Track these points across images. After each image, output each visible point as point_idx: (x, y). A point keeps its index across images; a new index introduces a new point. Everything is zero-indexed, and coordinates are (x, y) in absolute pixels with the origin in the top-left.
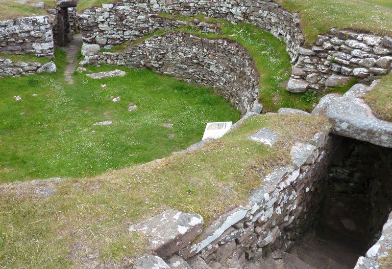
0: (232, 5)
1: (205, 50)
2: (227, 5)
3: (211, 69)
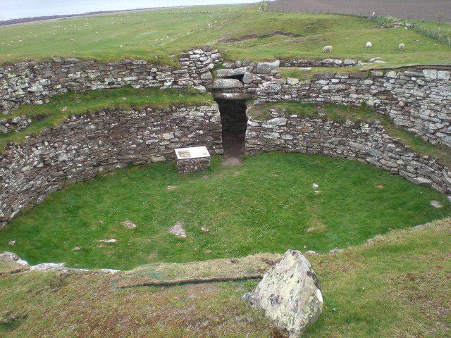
0: (28, 83)
1: (46, 144)
2: (23, 86)
3: (61, 159)
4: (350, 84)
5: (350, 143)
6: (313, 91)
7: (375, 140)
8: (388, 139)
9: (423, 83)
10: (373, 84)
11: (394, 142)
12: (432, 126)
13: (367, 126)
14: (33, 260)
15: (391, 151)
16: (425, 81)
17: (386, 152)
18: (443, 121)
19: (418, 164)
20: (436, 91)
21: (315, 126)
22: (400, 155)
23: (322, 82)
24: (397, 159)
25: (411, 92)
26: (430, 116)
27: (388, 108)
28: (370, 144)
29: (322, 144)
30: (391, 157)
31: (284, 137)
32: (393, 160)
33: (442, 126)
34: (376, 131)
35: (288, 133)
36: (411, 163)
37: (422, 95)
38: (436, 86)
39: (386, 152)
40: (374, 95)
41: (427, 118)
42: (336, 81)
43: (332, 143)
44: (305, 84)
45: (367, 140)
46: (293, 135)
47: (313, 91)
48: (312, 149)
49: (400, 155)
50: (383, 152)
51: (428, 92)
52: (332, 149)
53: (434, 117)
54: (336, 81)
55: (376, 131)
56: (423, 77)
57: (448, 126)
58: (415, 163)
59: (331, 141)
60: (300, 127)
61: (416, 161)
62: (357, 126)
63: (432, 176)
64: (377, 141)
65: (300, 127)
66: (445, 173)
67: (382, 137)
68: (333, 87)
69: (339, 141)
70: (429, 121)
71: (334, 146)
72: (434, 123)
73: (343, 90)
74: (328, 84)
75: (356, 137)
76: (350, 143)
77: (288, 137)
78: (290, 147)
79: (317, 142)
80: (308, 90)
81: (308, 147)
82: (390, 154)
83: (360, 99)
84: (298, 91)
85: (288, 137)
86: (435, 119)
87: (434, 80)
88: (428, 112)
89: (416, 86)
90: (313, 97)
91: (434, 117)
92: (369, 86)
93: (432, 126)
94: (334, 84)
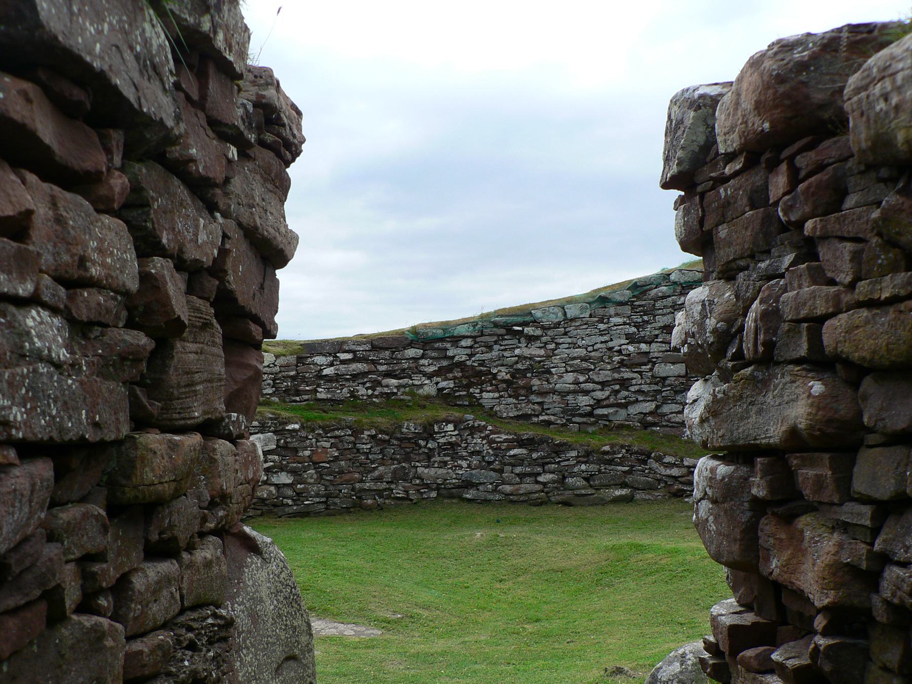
4: (373, 362)
5: (420, 470)
6: (304, 380)
7: (472, 454)
8: (506, 441)
9: (539, 332)
10: (423, 357)
11: (521, 443)
12: (584, 401)
13: (450, 427)
14: (783, 210)
15: (518, 461)
16: (543, 328)
17: (508, 468)
18: (604, 384)
19: (593, 468)
20: (569, 340)
21: (340, 446)
22: (543, 465)
23: (319, 360)
24: (539, 474)
25: (517, 352)
26: (576, 383)
27: (475, 391)
28: (464, 464)
29: (358, 485)
30: (522, 476)
31: (275, 479)
32: (528, 479)
33: (607, 393)
34: (472, 434)
35: (282, 469)
36: (576, 470)
37: (542, 352)
38: (566, 334)
39: (508, 468)
40: (430, 376)
41: (572, 387)
42: (349, 356)
43: (379, 479)
44: (288, 366)
45: (455, 457)
46: (293, 472)
47: (304, 380)
48: (337, 501)
49: (543, 465)
50: (501, 471)
51: (553, 346)
52: (380, 493)
53: (586, 382)
54: (349, 356)
55: (472, 434)
56: (535, 322)
57: (618, 392)
58: (583, 467)
59: (377, 473)
60: (307, 453)
61: (585, 463)
62: (428, 432)
63: (629, 479)
64: (478, 453)
65: (307, 453)
66: (655, 465)
67: (491, 442)
68: (342, 368)
69: (394, 472)
70: (575, 392)
71: (384, 485)
72: (586, 392)
73: (364, 374)
74: (331, 365)
75: (429, 456)
76: (420, 470)
77: (284, 478)
78: (290, 502)
79: (347, 482)
80: (293, 378)
81: (328, 496)
82: (518, 470)
83: (404, 386)
84: (274, 380)
85: (284, 478)
86: (590, 386)
87: (559, 323)
88: (570, 377)
89: (523, 340)
90: (306, 392)
91: (586, 382)
92: (415, 359)
93: (584, 401)
94: (343, 362)
